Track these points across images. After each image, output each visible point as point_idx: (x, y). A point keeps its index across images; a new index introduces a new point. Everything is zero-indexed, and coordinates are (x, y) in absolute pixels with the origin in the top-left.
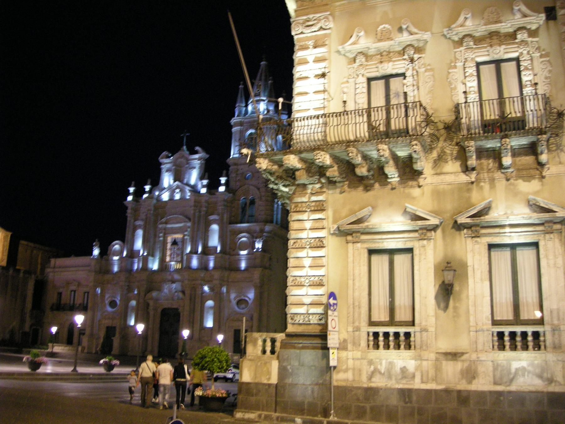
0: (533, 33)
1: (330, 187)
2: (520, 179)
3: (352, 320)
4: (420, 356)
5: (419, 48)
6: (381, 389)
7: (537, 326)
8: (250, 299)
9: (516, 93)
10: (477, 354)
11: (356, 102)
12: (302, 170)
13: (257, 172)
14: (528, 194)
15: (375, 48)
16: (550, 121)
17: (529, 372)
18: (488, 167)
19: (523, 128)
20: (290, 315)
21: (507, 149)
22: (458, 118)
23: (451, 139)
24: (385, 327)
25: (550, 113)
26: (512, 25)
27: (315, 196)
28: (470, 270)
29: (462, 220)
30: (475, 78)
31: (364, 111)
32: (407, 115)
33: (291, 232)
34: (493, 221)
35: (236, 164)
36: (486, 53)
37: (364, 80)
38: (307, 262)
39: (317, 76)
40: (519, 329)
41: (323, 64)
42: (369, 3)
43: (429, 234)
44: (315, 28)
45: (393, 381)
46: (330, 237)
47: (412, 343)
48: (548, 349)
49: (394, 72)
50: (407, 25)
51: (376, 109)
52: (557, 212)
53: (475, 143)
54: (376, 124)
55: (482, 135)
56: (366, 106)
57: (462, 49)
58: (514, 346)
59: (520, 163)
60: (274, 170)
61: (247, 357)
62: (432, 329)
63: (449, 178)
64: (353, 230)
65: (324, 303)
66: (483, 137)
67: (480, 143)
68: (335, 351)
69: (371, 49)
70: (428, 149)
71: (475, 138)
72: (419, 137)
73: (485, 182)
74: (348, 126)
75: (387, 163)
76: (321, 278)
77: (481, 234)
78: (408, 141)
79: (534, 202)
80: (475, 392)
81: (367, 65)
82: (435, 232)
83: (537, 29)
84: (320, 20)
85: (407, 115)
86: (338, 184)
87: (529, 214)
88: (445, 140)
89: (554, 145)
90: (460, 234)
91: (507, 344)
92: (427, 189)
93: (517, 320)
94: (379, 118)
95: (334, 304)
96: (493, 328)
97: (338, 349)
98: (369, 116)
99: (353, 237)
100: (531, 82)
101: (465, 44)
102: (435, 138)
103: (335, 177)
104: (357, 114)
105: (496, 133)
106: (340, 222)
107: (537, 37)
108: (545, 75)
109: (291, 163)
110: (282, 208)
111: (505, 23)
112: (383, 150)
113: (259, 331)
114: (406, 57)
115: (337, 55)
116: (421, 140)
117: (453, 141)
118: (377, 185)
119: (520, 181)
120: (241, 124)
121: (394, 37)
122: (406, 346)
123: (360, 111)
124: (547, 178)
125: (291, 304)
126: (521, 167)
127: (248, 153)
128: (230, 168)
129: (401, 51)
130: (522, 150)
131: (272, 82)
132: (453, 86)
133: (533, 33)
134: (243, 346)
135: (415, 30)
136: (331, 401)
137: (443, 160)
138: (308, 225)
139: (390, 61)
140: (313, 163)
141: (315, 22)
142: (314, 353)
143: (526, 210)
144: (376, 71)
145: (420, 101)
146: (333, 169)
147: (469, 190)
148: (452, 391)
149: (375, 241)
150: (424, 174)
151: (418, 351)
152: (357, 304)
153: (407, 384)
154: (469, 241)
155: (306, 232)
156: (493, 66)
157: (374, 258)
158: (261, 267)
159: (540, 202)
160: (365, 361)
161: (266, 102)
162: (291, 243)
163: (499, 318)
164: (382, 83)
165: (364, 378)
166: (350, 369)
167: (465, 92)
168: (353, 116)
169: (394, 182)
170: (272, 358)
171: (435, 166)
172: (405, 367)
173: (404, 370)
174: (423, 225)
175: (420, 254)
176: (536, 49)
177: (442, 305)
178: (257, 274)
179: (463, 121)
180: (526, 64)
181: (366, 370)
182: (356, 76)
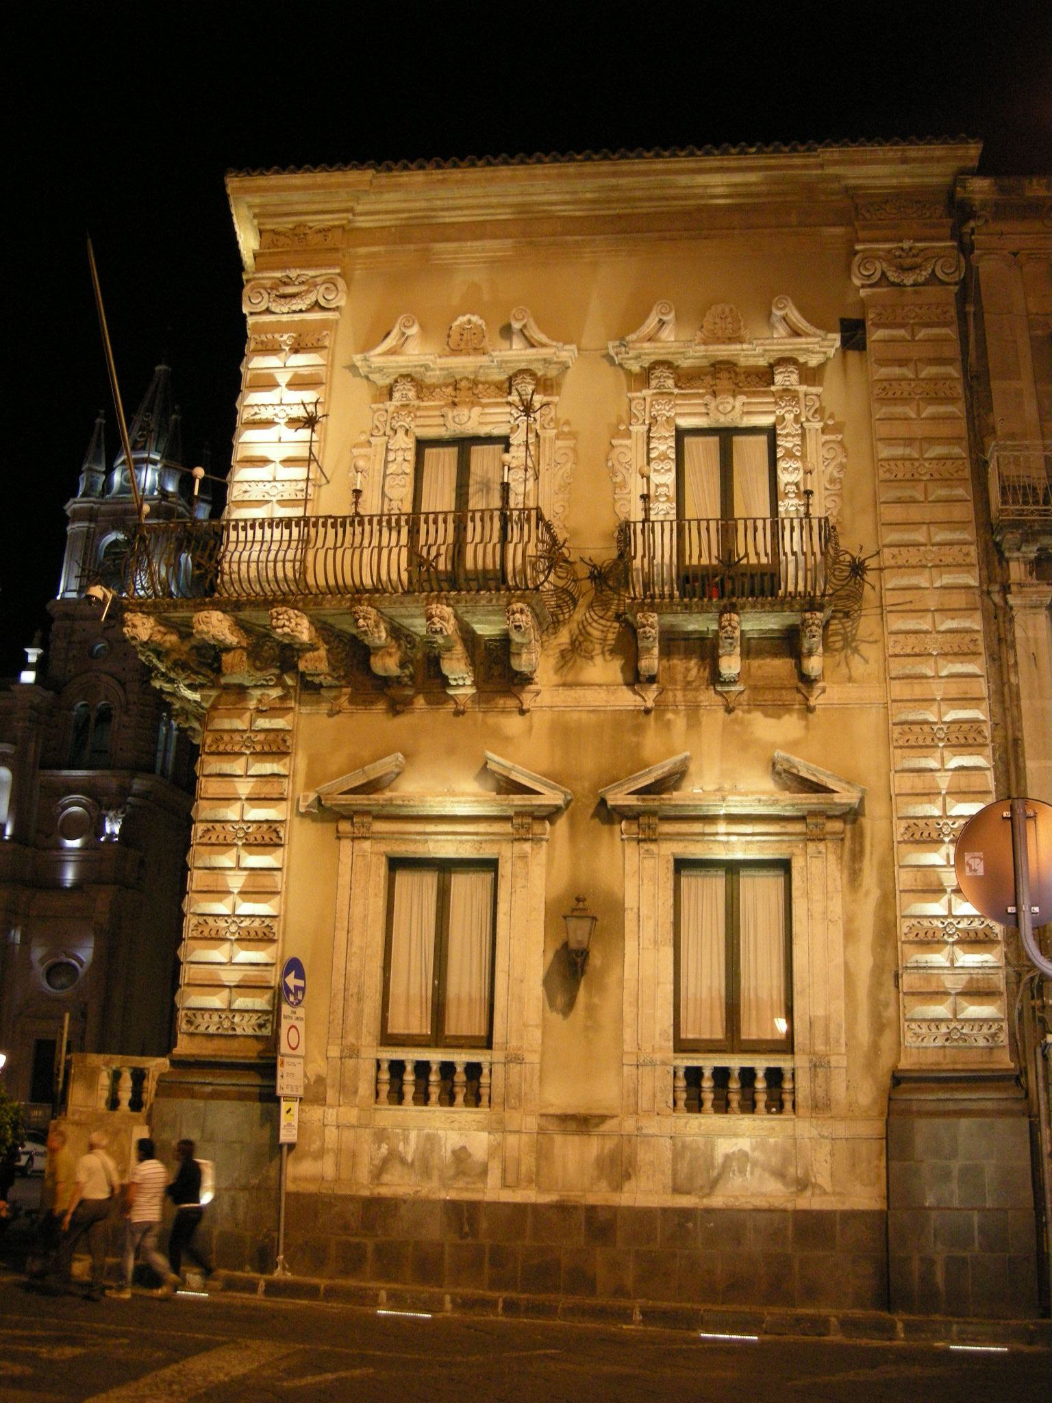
0: (811, 375)
1: (305, 697)
3: (339, 1031)
4: (501, 1122)
5: (546, 380)
6: (405, 1202)
7: (778, 1056)
8: (81, 962)
9: (762, 509)
10: (637, 1121)
11: (383, 494)
12: (239, 651)
13: (124, 647)
14: (774, 746)
15: (442, 369)
16: (834, 580)
17: (755, 1164)
18: (685, 677)
19: (773, 594)
20: (185, 1012)
21: (732, 638)
22: (624, 556)
23: (605, 605)
24: (420, 1050)
25: (835, 563)
26: (765, 351)
27: (266, 717)
28: (630, 918)
29: (619, 797)
30: (673, 466)
31: (403, 518)
32: (504, 539)
34: (689, 806)
35: (68, 616)
36: (703, 410)
37: (411, 443)
38: (236, 882)
39: (293, 422)
40: (735, 1062)
41: (309, 396)
42: (439, 259)
43: (537, 828)
45: (435, 1183)
46: (297, 820)
47: (484, 1091)
48: (800, 1111)
49: (483, 431)
51: (431, 517)
53: (659, 620)
54: (428, 553)
55: (677, 600)
56: (408, 508)
57: (645, 392)
58: (723, 1103)
60: (168, 645)
61: (70, 1116)
62: (533, 1058)
64: (355, 808)
65: (272, 984)
66: (678, 605)
67: (669, 619)
68: (295, 1106)
69: (433, 370)
70: (548, 624)
71: (661, 605)
72: (529, 592)
73: (676, 712)
74: (362, 552)
75: (449, 649)
76: (267, 921)
77: (660, 834)
78: (503, 601)
79: (786, 766)
80: (630, 1209)
81: (418, 408)
82: (552, 823)
83: (822, 366)
84: (316, 285)
85: (504, 539)
86: (323, 692)
89: (839, 638)
90: (612, 833)
91: (708, 1097)
92: (540, 720)
93: (733, 1041)
94: (437, 539)
95: (297, 988)
96: (675, 1058)
97: (301, 1099)
98: (414, 533)
99: (353, 824)
100: (798, 487)
101: (654, 383)
102: (567, 597)
103: (319, 675)
104: (384, 524)
105: (710, 598)
106: (324, 787)
107: (821, 385)
109: (213, 631)
110: (178, 738)
111: (751, 343)
112: (442, 618)
113: (101, 1050)
114: (514, 398)
115: (348, 374)
116: (534, 602)
117: (608, 610)
118: (420, 702)
119: (757, 716)
120: (91, 515)
121: (489, 349)
122: (469, 1097)
123: (394, 519)
124: (817, 712)
125: (189, 985)
126: (761, 683)
127: (105, 596)
128: (54, 626)
129: (502, 383)
130: (765, 642)
131: (179, 418)
132: (619, 479)
133: (811, 375)
134: (61, 1086)
135: (542, 337)
136: (278, 1230)
139: (473, 404)
140: (267, 635)
141: (303, 288)
142: (242, 1110)
143: (767, 784)
144: (439, 425)
145: (538, 509)
146: (316, 653)
147: (639, 729)
148: (575, 1208)
149: (407, 836)
150: (537, 684)
151: (498, 1109)
152: (353, 989)
153: (467, 1190)
154: (631, 849)
155: (237, 806)
156: (714, 440)
157: (404, 880)
158: (114, 884)
159: (800, 768)
160: (368, 1131)
161: (159, 466)
162: (199, 828)
163: (690, 1036)
164: (451, 453)
165: (363, 1175)
166: (329, 1150)
167: (645, 497)
168: (376, 527)
170: (133, 1118)
171: (562, 666)
172: (464, 1148)
173: (461, 1155)
174: (525, 806)
176: (816, 412)
177: (560, 1000)
178: (103, 900)
179: (637, 563)
180: (790, 445)
181: (370, 1152)
182: (389, 432)
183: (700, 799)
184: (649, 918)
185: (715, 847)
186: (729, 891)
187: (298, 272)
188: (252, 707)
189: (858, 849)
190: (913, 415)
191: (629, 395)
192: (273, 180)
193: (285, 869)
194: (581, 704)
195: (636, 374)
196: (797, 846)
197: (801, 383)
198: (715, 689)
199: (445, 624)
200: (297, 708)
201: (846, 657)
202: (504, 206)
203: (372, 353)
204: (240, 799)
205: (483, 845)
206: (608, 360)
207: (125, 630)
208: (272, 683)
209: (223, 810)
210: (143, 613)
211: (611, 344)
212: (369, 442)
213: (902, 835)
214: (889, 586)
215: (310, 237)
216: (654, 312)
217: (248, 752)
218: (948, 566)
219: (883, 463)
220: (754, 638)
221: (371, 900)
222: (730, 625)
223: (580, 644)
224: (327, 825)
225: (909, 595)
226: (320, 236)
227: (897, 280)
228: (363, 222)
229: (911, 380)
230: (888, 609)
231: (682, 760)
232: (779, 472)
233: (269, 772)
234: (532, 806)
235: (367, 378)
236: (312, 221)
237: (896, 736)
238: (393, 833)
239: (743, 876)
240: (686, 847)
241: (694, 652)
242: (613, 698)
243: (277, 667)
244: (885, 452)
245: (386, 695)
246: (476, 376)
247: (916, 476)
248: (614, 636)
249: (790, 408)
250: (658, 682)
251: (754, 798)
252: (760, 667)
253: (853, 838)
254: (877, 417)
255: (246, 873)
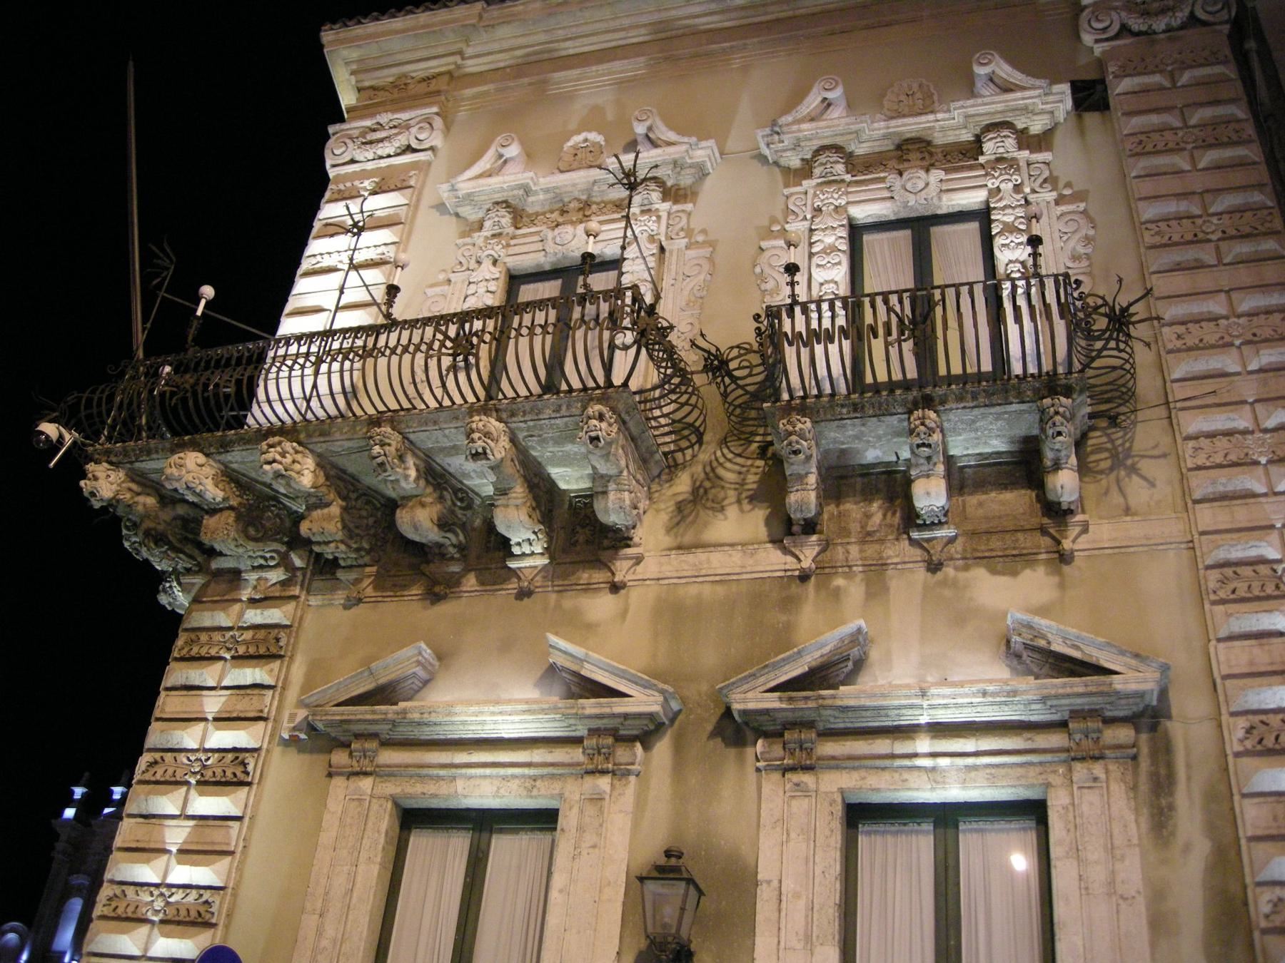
2: (978, 565)
12: (226, 513)
15: (547, 191)
26: (967, 117)
28: (765, 895)
30: (845, 260)
33: (155, 727)
34: (865, 709)
36: (887, 194)
43: (622, 754)
44: (388, 148)
46: (277, 751)
50: (648, 123)
52: (1116, 673)
57: (806, 183)
59: (981, 512)
63: (718, 562)
66: (843, 406)
69: (536, 193)
73: (849, 576)
76: (207, 895)
77: (819, 759)
82: (647, 747)
86: (340, 574)
87: (1006, 682)
88: (724, 442)
90: (741, 760)
92: (639, 598)
99: (351, 755)
101: (817, 171)
108: (1074, 249)
112: (487, 435)
115: (435, 213)
116: (621, 406)
118: (471, 582)
119: (980, 574)
124: (1077, 562)
126: (984, 527)
127: (61, 436)
130: (988, 470)
137: (709, 504)
138: (212, 704)
143: (1000, 672)
147: (789, 604)
154: (772, 785)
156: (905, 235)
169: (526, 572)
171: (678, 524)
175: (581, 829)
176: (1045, 181)
183: (884, 696)
184: (797, 895)
185: (914, 779)
186: (941, 856)
187: (390, 116)
188: (244, 599)
189: (1163, 772)
190: (1187, 167)
191: (786, 191)
192: (371, 27)
193: (246, 820)
194: (703, 572)
195: (796, 170)
196: (1055, 772)
197: (1020, 148)
198: (910, 539)
199: (492, 444)
200: (303, 597)
201: (1118, 481)
202: (637, 27)
203: (460, 178)
204: (206, 720)
205: (538, 783)
206: (759, 161)
207: (82, 483)
208: (272, 563)
209: (178, 733)
210: (111, 463)
211: (760, 133)
212: (449, 281)
213: (1241, 741)
214: (1176, 375)
215: (411, 86)
216: (815, 90)
217: (228, 656)
218: (1266, 340)
219: (1149, 226)
220: (970, 466)
221: (362, 867)
222: (923, 424)
223: (706, 492)
224: (315, 756)
225: (1209, 385)
226: (424, 84)
227: (1144, 28)
228: (472, 66)
229: (1177, 129)
230: (1179, 405)
231: (852, 635)
232: (996, 251)
233: (249, 681)
234: (614, 716)
235: (457, 215)
236: (415, 71)
237: (1212, 585)
238: (407, 766)
239: (964, 831)
240: (863, 779)
241: (878, 491)
242: (751, 562)
243: (283, 543)
244: (1149, 211)
245: (424, 574)
246: (590, 196)
247: (1201, 236)
248: (756, 478)
249: (1007, 177)
250: (821, 532)
251: (974, 689)
252: (980, 504)
253: (1154, 755)
254: (1133, 174)
255: (192, 823)
